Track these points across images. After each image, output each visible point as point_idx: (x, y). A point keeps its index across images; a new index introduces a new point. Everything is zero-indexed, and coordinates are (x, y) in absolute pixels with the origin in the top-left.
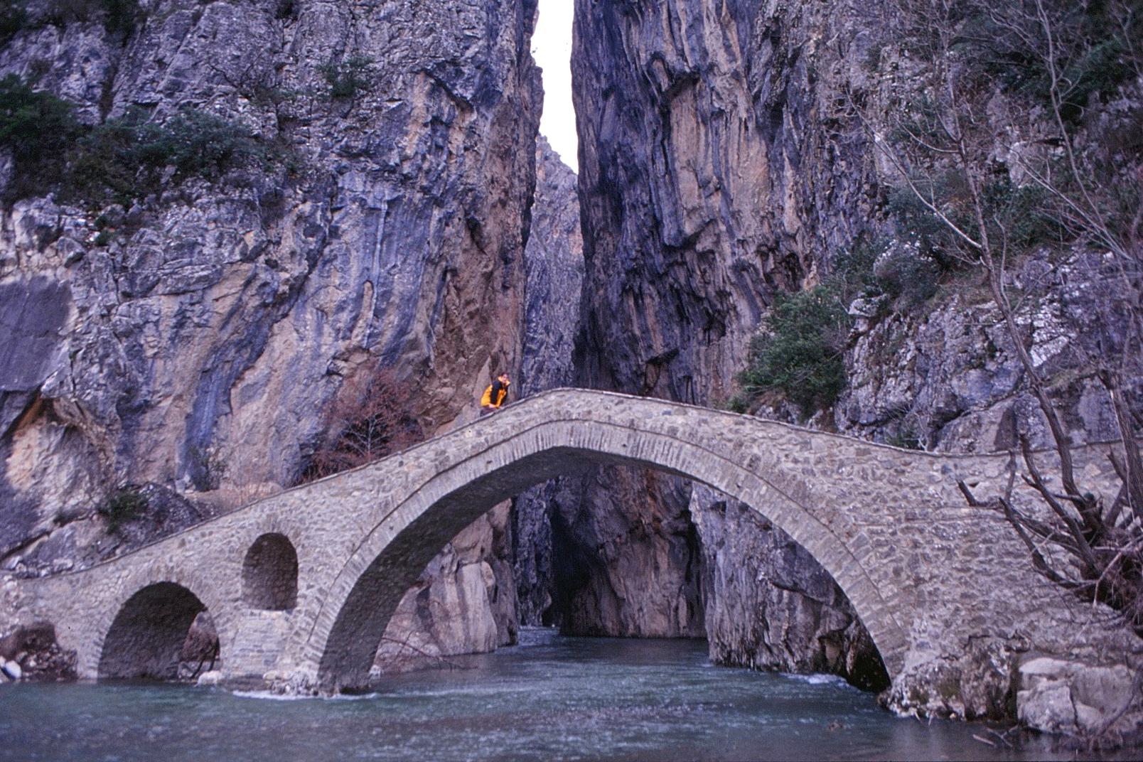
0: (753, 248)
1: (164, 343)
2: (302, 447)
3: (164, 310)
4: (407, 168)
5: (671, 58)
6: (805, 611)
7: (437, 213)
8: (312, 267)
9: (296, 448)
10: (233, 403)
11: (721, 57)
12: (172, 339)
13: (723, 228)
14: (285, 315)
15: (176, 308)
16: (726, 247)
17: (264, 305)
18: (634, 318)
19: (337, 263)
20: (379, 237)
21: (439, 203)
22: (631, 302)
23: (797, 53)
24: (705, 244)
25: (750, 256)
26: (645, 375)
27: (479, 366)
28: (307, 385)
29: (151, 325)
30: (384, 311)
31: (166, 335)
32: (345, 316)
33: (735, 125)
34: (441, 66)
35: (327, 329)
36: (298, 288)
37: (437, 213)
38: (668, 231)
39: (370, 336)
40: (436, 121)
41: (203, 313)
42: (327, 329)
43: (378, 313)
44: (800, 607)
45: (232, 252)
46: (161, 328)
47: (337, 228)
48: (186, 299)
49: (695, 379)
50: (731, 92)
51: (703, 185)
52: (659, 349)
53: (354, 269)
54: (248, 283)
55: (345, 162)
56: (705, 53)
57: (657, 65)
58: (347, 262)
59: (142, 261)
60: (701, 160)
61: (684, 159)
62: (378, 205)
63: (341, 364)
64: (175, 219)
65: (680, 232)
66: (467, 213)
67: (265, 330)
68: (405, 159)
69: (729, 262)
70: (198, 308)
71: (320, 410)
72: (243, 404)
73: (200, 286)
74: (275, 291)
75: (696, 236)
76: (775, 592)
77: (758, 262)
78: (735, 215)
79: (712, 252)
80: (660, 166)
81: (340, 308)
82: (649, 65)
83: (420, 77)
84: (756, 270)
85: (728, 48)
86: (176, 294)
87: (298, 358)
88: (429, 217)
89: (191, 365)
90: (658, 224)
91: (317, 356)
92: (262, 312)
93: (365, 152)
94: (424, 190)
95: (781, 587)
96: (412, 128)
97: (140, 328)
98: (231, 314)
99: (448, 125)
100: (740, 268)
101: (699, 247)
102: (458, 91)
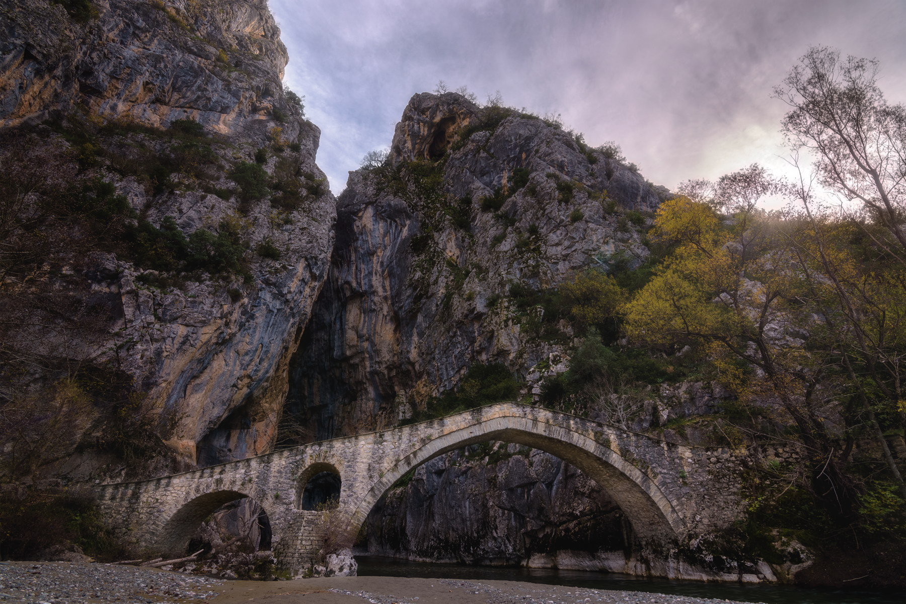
1: (174, 350)
2: (211, 422)
3: (179, 333)
4: (289, 297)
5: (354, 284)
6: (515, 520)
11: (380, 290)
12: (178, 350)
14: (221, 351)
15: (185, 333)
17: (217, 344)
19: (250, 331)
21: (294, 317)
23: (433, 294)
31: (176, 346)
32: (247, 358)
33: (381, 316)
34: (312, 258)
37: (292, 321)
38: (336, 353)
40: (303, 280)
42: (238, 363)
43: (261, 360)
48: (191, 329)
50: (381, 303)
51: (360, 337)
52: (317, 401)
55: (264, 286)
56: (371, 286)
57: (347, 286)
58: (254, 332)
59: (173, 303)
60: (361, 326)
61: (351, 325)
64: (194, 287)
68: (290, 292)
70: (194, 336)
72: (192, 393)
75: (351, 357)
76: (501, 511)
77: (386, 372)
79: (357, 365)
80: (338, 326)
81: (246, 354)
82: (342, 285)
83: (303, 260)
84: (383, 374)
85: (384, 287)
87: (223, 374)
89: (180, 366)
90: (331, 349)
91: (232, 375)
93: (274, 284)
94: (291, 309)
95: (504, 509)
96: (295, 280)
98: (206, 343)
99: (306, 284)
102: (314, 270)
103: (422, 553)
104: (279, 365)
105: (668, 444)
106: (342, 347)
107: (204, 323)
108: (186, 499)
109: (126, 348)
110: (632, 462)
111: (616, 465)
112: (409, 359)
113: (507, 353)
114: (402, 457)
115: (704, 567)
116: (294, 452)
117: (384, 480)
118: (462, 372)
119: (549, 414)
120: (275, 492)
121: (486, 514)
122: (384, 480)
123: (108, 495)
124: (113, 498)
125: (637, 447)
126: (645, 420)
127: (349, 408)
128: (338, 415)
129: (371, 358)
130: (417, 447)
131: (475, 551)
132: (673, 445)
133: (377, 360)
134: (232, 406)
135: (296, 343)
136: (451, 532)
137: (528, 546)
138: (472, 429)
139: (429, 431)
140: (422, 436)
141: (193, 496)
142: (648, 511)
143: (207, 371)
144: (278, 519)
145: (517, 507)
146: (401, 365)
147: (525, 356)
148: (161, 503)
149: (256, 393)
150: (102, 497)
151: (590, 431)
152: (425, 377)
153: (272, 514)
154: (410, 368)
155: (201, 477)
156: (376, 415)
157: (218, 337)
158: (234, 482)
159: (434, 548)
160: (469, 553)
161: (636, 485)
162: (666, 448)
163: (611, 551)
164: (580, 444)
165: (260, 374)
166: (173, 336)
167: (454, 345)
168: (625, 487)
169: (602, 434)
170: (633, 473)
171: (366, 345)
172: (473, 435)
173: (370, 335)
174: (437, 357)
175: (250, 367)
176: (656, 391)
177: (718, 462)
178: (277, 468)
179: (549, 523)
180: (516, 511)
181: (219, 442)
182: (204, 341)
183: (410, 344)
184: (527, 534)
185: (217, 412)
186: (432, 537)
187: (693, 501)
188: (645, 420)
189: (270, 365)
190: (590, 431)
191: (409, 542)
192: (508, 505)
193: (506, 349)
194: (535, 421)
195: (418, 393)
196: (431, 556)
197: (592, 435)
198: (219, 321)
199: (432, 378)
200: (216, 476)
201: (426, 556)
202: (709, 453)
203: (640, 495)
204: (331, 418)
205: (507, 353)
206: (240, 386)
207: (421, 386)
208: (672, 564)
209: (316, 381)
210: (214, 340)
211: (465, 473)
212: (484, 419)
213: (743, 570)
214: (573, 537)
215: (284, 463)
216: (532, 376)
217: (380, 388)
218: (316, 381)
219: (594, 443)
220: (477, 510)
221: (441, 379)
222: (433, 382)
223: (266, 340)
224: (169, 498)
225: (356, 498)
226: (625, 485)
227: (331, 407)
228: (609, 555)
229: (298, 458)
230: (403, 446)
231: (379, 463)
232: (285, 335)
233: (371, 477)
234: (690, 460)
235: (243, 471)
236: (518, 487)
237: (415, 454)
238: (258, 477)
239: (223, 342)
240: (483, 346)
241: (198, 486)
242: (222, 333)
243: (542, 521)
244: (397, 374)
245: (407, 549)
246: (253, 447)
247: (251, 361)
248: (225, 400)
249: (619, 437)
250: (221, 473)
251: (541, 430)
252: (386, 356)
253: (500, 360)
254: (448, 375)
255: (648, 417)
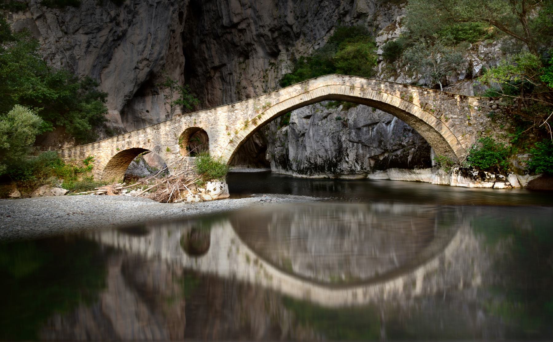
0: (267, 29)
1: (83, 54)
7: (172, 9)
8: (129, 26)
9: (123, 97)
10: (102, 78)
12: (85, 52)
13: (252, 21)
14: (119, 45)
15: (87, 40)
16: (253, 27)
17: (114, 40)
18: (206, 52)
19: (138, 25)
20: (154, 16)
22: (204, 46)
24: (243, 26)
25: (266, 31)
26: (209, 72)
27: (176, 67)
28: (128, 73)
29: (77, 46)
30: (155, 45)
31: (84, 50)
32: (141, 46)
35: (134, 51)
36: (125, 33)
37: (172, 9)
38: (225, 21)
39: (150, 54)
41: (96, 42)
43: (153, 46)
44: (361, 148)
45: (106, 18)
46: (81, 47)
47: (138, 12)
48: (90, 36)
49: (234, 74)
52: (217, 63)
53: (145, 27)
54: (111, 30)
58: (142, 25)
62: (153, 4)
63: (140, 65)
65: (231, 21)
66: (180, 9)
67: (112, 50)
69: (255, 33)
70: (94, 40)
71: (132, 82)
72: (106, 79)
73: (95, 31)
74: (118, 35)
75: (238, 23)
76: (351, 144)
77: (269, 34)
78: (259, 17)
79: (245, 29)
84: (268, 36)
86: (87, 34)
88: (169, 10)
90: (220, 18)
92: (113, 43)
95: (353, 142)
97: (74, 47)
98: (104, 43)
100: (260, 36)
101: (240, 27)
103: (300, 171)
104: (170, 45)
105: (461, 97)
106: (229, 16)
107: (99, 29)
108: (112, 154)
109: (49, 58)
110: (431, 111)
111: (416, 115)
112: (287, 22)
113: (365, 15)
114: (250, 120)
115: (471, 179)
116: (173, 121)
117: (239, 135)
118: (332, 32)
119: (363, 81)
120: (166, 147)
121: (341, 146)
122: (239, 135)
123: (66, 155)
124: (70, 156)
125: (435, 100)
126: (462, 74)
127: (244, 66)
128: (236, 72)
129: (255, 23)
130: (260, 112)
131: (335, 170)
132: (465, 97)
133: (261, 24)
134: (139, 82)
135: (181, 24)
136: (318, 157)
137: (372, 165)
138: (301, 97)
139: (268, 100)
140: (264, 104)
141: (116, 152)
142: (442, 144)
143: (112, 62)
144: (171, 163)
145: (363, 141)
146: (281, 27)
147: (379, 18)
148: (98, 157)
149: (156, 70)
150: (63, 156)
151: (397, 91)
152: (302, 36)
153: (167, 160)
154: (289, 29)
155: (118, 140)
156: (266, 71)
157: (113, 35)
158: (139, 142)
159: (307, 169)
160: (331, 171)
161: (431, 127)
162: (459, 100)
163: (423, 168)
164: (388, 101)
165: (155, 56)
166: (79, 43)
167: (323, 8)
168: (426, 128)
169: (406, 92)
170: (429, 120)
171: (249, 12)
172: (302, 101)
173: (251, 3)
174: (310, 19)
175: (145, 52)
176: (475, 49)
177: (498, 108)
178: (164, 133)
179: (386, 151)
180: (362, 143)
181: (138, 107)
182: (103, 42)
183: (286, 9)
184: (371, 158)
185: (129, 88)
186: (306, 162)
187: (474, 136)
188: (462, 74)
189: (162, 48)
190: (397, 91)
191: (292, 165)
192: (356, 139)
193: (365, 12)
194: (352, 88)
195: (297, 51)
196: (306, 174)
197: (398, 93)
198: (110, 25)
199: (308, 38)
200: (127, 140)
201: (303, 174)
202: (492, 102)
203: (436, 134)
204: (231, 74)
205: (365, 15)
206: (141, 68)
207: (300, 44)
208: (454, 177)
209: (212, 46)
210: (111, 39)
211: (326, 117)
212: (310, 89)
213: (498, 180)
214: (399, 160)
215: (168, 129)
216: (380, 37)
217: (267, 48)
218: (212, 46)
219: (400, 99)
220: (335, 143)
221: (315, 39)
222: (309, 41)
223: (152, 30)
224: (102, 154)
225: (221, 148)
226: (423, 128)
227: (229, 66)
228: (421, 171)
229: (177, 125)
230: (250, 113)
231: (233, 125)
232: (169, 21)
233: (229, 134)
234: (476, 108)
235: (143, 136)
236: (364, 126)
237: (260, 118)
238: (153, 138)
239: (119, 38)
240: (346, 9)
241: (117, 146)
242: (115, 32)
243: (382, 149)
244: (279, 35)
245: (291, 169)
246: (164, 108)
247: (145, 47)
248: (132, 79)
249: (421, 94)
250: (129, 137)
251: (357, 93)
252: (268, 21)
253: (360, 22)
254: (320, 34)
255: (464, 72)
